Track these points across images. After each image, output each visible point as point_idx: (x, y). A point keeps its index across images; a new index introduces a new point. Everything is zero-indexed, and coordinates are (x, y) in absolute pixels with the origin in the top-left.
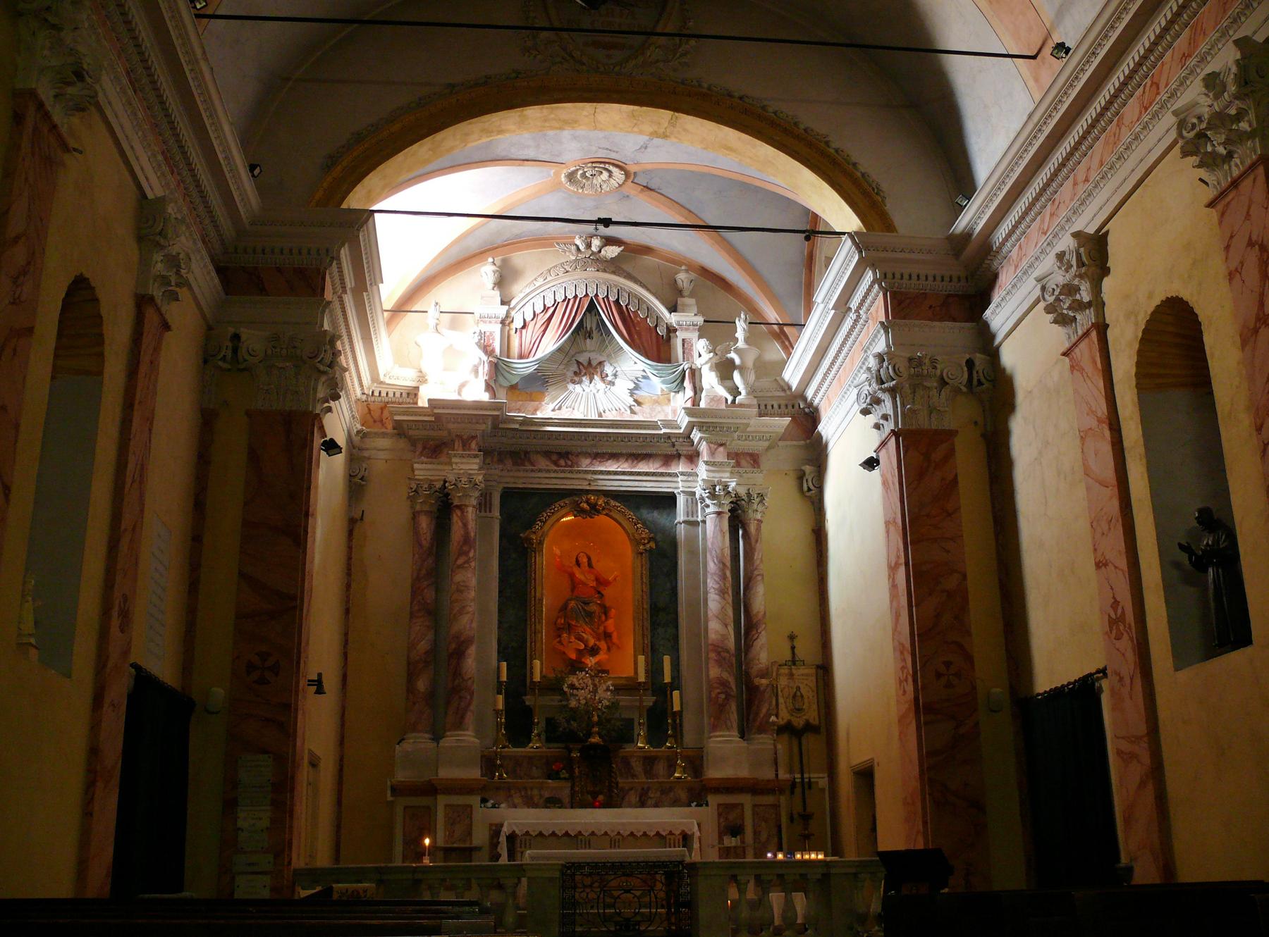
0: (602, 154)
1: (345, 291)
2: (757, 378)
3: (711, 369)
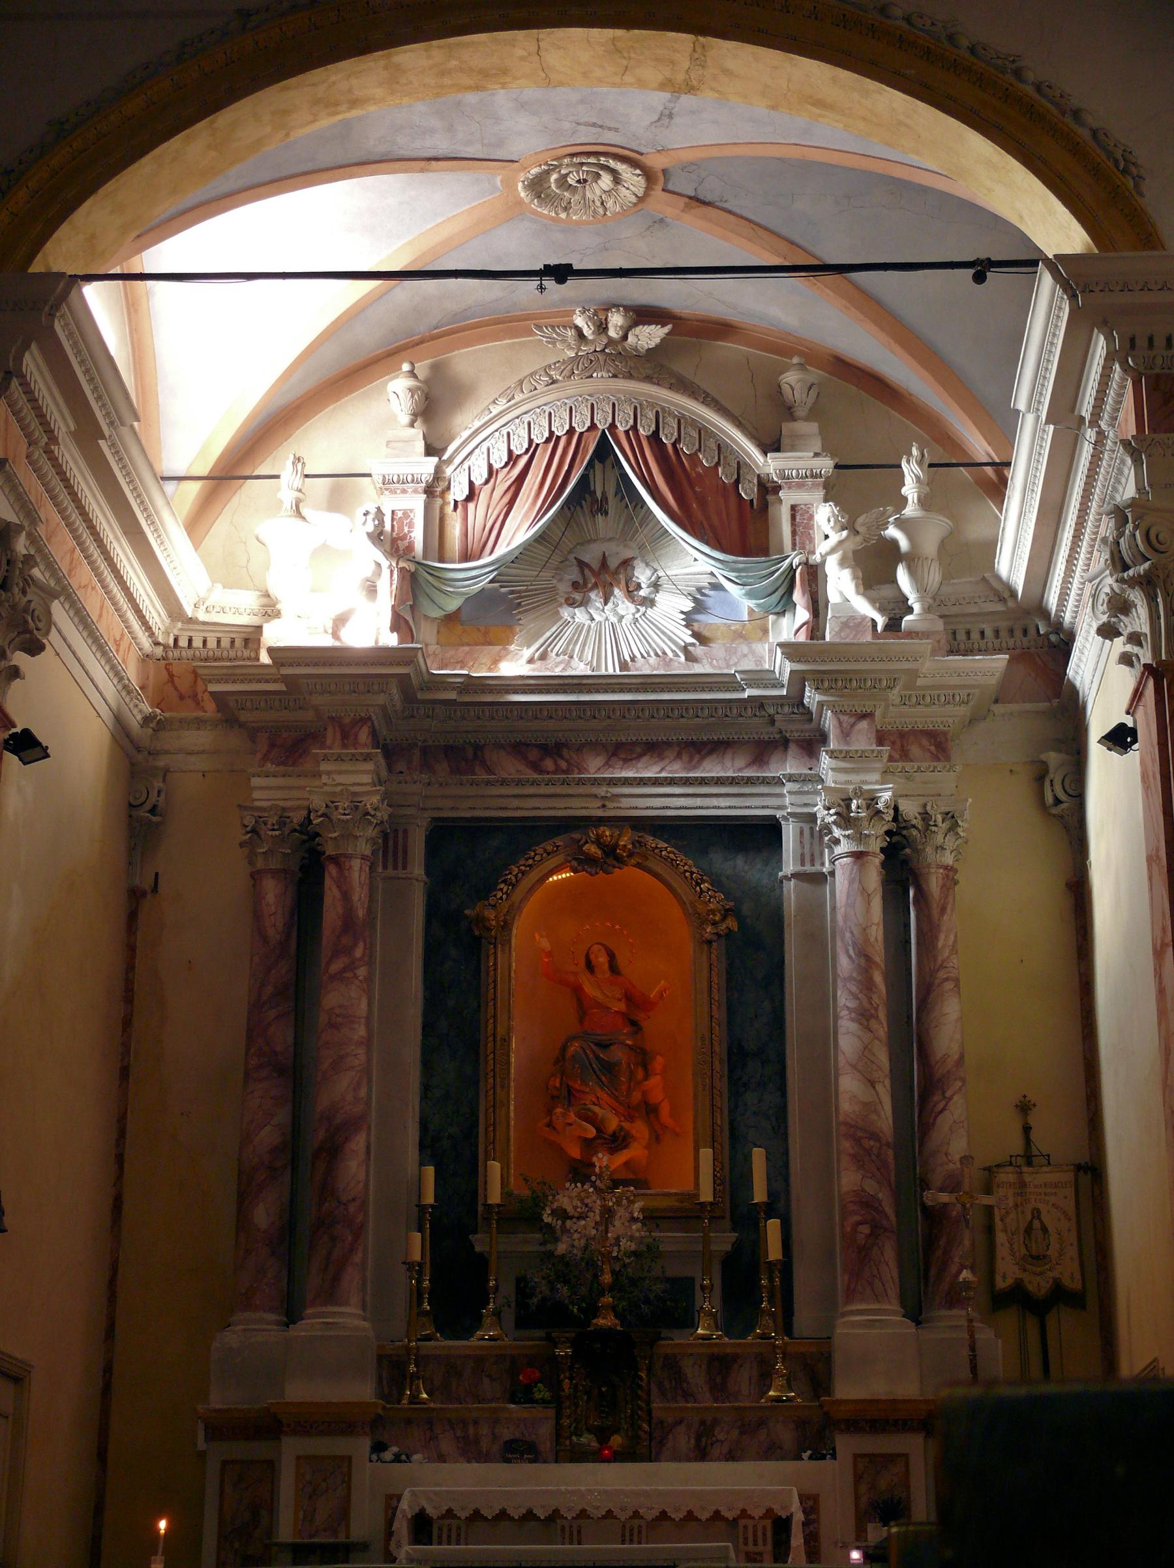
0: (585, 136)
1: (53, 439)
2: (947, 577)
3: (843, 563)
